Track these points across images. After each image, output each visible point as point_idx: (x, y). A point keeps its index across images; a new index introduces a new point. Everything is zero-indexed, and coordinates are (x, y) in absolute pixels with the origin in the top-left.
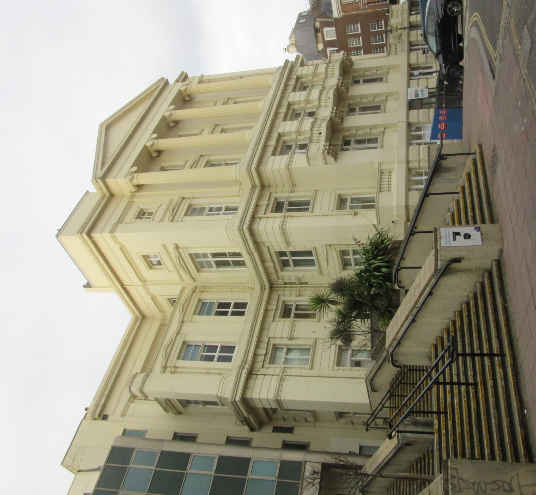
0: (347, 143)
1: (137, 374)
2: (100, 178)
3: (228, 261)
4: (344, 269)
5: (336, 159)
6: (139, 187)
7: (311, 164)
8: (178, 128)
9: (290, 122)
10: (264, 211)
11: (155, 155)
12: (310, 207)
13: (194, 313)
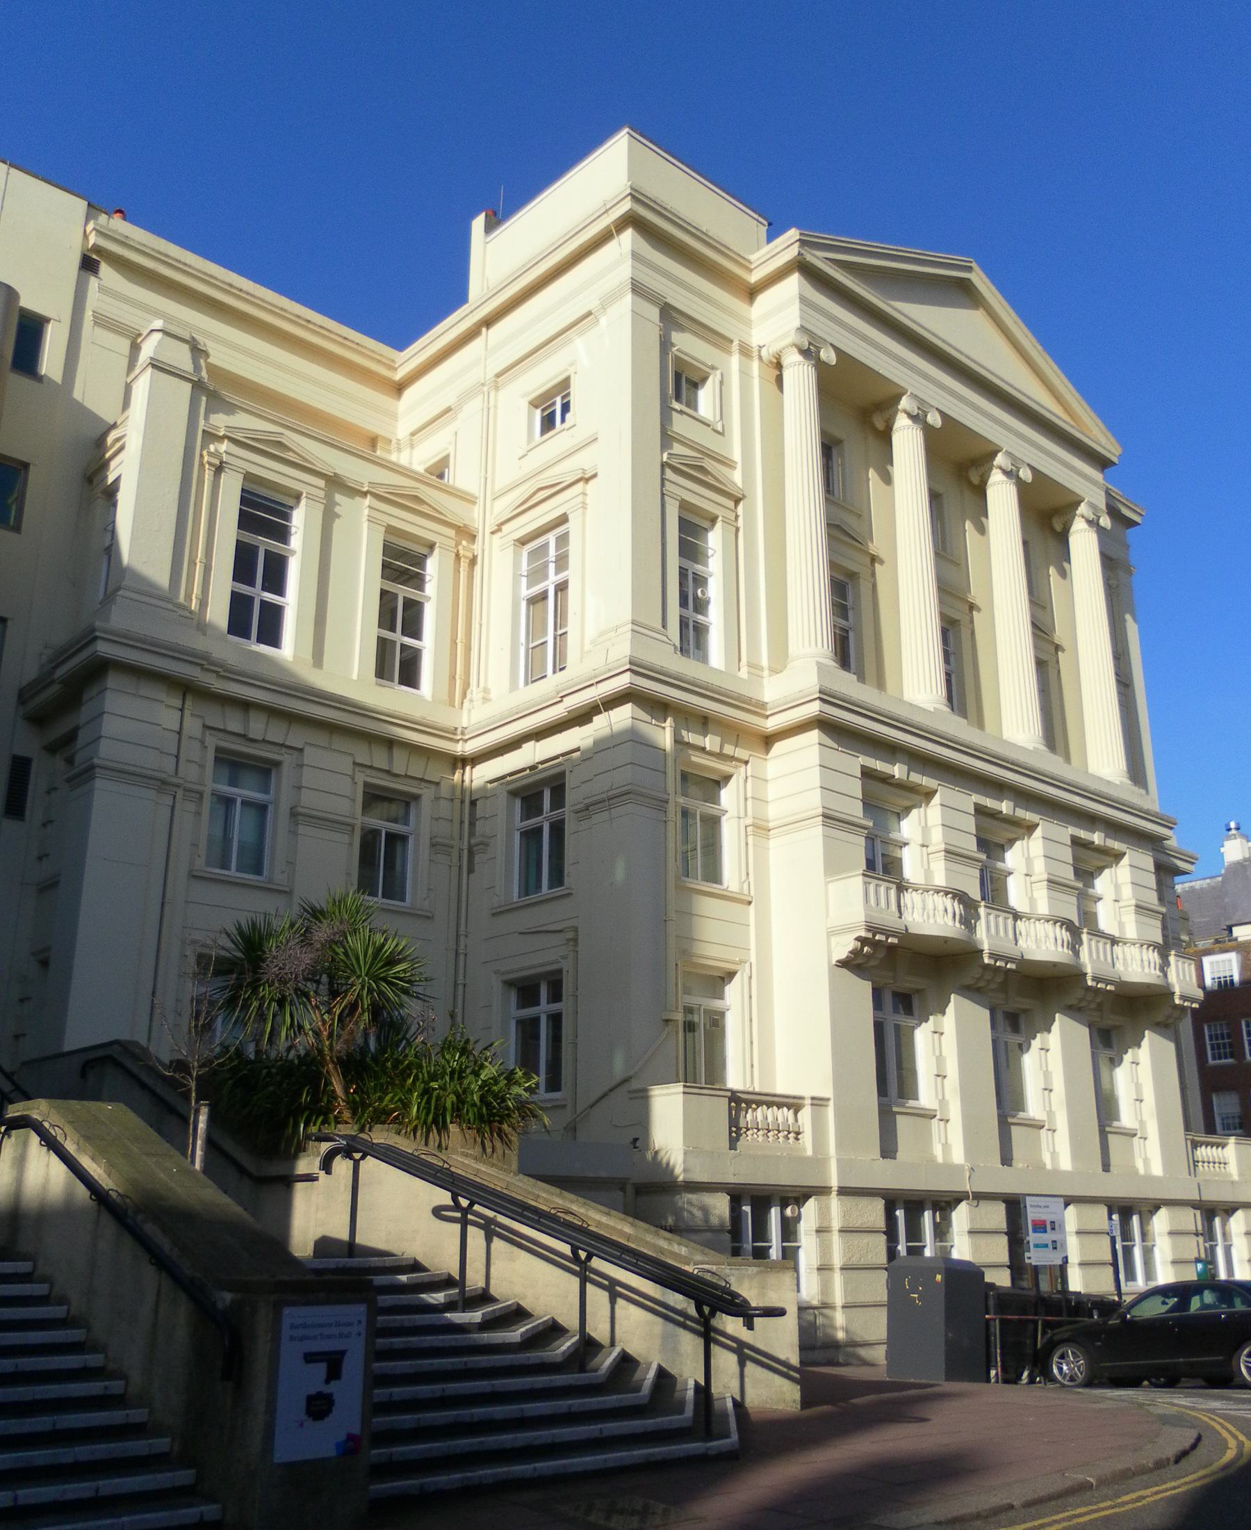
5: (844, 964)
7: (437, 781)
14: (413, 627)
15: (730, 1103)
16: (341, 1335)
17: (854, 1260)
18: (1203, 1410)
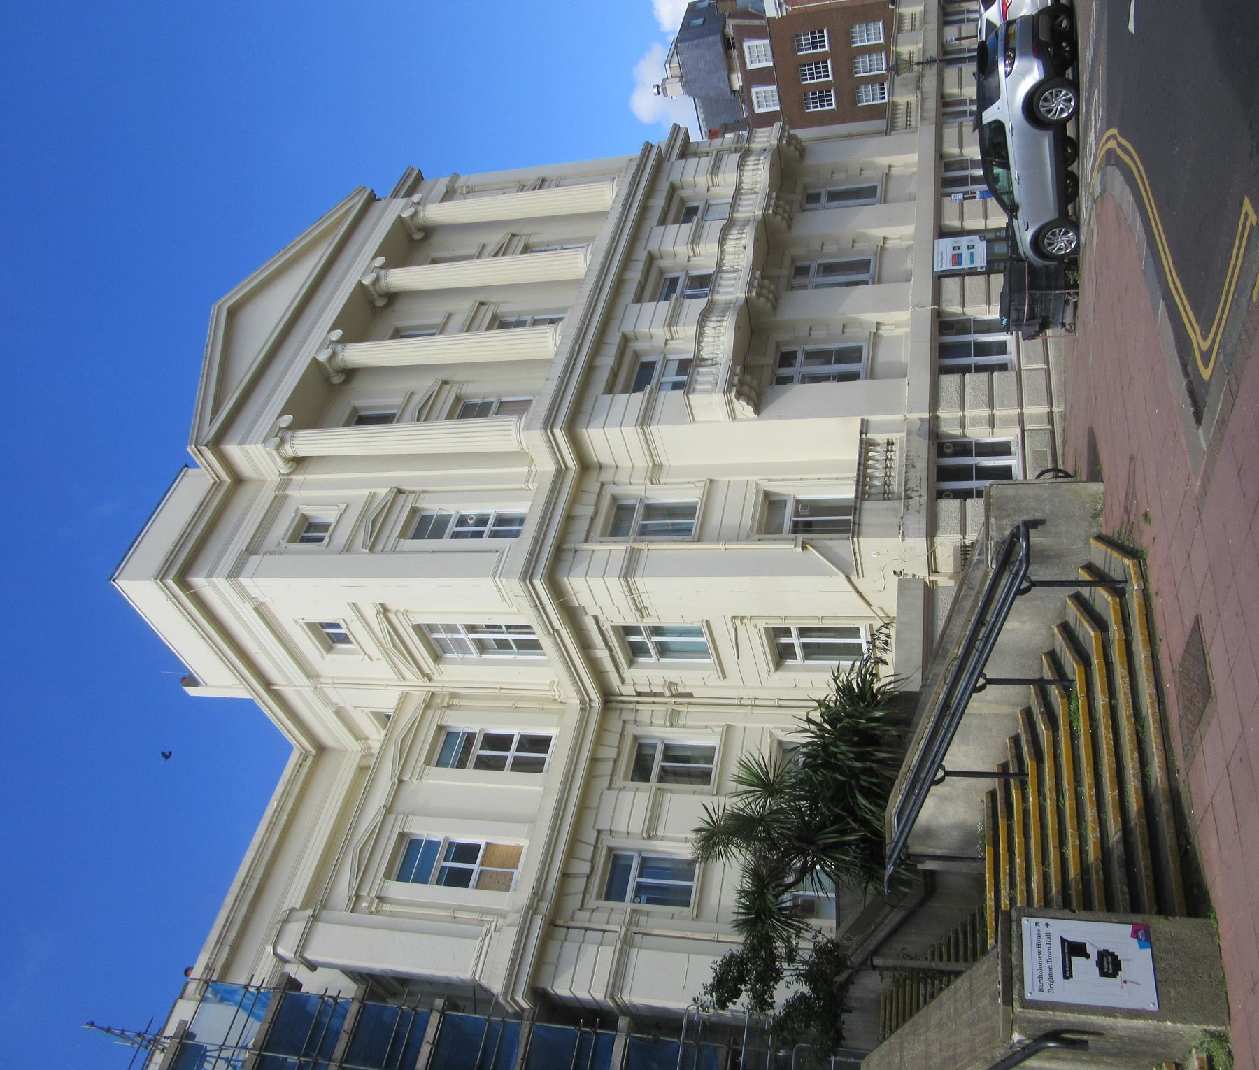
0: (802, 271)
1: (293, 910)
2: (206, 445)
3: (507, 640)
4: (778, 665)
5: (758, 410)
6: (298, 462)
7: (596, 832)
8: (394, 311)
9: (651, 303)
10: (584, 534)
11: (418, 236)
12: (695, 521)
13: (428, 762)
14: (500, 742)
15: (866, 500)
16: (1048, 943)
17: (986, 399)
18: (1097, 149)
